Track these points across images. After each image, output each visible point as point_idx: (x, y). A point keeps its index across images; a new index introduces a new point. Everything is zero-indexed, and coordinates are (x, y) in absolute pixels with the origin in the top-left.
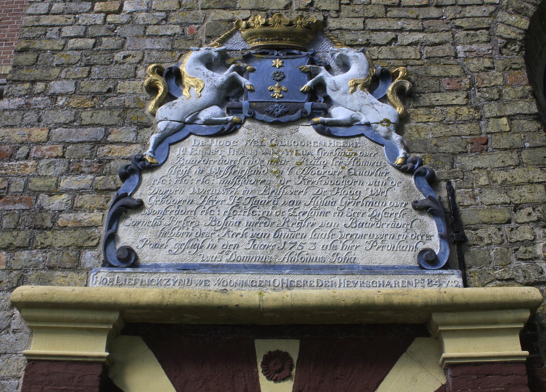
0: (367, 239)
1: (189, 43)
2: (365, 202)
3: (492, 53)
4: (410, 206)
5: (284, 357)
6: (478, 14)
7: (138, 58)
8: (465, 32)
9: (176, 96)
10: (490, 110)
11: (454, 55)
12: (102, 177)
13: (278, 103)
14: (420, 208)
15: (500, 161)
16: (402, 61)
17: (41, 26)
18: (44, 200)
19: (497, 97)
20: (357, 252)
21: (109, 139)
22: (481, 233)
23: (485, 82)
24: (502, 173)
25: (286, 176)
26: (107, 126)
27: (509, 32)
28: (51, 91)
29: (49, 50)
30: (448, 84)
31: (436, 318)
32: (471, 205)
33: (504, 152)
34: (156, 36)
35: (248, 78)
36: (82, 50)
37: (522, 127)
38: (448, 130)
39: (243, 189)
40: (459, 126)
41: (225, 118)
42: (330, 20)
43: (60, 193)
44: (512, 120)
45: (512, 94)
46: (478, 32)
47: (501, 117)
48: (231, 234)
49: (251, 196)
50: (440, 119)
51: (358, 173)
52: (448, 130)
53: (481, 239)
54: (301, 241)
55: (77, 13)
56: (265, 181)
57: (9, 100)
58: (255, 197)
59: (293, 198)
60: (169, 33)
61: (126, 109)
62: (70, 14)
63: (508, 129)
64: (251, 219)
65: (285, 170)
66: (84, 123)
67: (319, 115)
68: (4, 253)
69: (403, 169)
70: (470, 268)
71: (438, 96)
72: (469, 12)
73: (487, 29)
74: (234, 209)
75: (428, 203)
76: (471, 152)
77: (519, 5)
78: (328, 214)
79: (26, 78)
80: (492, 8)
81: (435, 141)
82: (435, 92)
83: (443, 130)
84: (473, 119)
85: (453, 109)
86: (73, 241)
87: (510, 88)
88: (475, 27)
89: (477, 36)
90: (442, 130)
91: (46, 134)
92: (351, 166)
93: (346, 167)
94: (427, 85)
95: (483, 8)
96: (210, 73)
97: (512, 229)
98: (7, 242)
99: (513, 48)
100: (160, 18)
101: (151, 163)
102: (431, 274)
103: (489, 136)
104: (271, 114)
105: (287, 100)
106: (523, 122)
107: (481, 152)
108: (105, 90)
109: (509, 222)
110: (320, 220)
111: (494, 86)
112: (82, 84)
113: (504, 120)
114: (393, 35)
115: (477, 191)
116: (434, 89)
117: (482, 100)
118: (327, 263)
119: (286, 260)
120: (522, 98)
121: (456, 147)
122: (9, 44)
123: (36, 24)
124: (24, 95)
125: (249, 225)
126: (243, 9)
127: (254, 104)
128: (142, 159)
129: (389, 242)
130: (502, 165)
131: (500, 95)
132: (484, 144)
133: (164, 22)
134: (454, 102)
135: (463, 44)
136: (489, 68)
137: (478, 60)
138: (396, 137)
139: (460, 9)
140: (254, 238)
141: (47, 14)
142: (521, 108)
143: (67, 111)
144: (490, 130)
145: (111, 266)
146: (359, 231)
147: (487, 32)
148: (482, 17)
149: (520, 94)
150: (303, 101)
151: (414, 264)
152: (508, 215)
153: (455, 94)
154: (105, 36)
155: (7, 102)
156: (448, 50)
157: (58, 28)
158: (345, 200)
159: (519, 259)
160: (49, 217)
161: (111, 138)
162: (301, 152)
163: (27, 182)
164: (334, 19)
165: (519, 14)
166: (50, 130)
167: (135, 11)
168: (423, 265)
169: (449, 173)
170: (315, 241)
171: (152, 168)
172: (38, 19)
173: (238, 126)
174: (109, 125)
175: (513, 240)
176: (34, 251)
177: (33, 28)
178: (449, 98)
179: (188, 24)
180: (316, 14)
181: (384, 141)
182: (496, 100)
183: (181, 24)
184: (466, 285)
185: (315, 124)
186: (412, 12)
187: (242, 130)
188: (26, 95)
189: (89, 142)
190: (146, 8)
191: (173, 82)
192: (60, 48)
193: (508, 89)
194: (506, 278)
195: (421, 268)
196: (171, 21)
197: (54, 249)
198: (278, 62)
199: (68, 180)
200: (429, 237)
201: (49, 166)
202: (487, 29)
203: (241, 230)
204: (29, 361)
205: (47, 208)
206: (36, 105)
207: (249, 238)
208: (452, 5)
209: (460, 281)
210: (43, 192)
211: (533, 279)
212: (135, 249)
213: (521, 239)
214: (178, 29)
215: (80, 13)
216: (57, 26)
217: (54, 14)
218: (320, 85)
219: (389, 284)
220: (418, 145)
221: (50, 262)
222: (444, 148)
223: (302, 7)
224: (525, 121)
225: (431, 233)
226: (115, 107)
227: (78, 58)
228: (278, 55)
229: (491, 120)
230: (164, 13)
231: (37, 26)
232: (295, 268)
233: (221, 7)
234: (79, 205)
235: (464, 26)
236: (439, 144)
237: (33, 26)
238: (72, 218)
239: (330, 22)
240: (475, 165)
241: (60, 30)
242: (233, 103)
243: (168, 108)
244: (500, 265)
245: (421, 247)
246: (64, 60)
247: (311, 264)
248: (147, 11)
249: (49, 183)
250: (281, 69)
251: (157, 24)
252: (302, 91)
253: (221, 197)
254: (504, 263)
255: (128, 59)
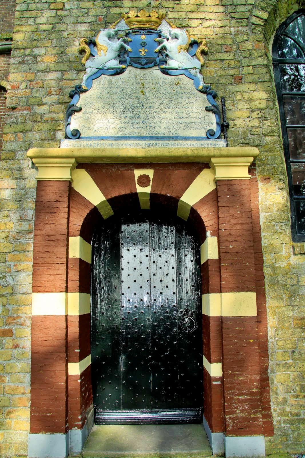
0: (184, 124)
1: (99, 26)
2: (183, 107)
3: (248, 32)
4: (204, 109)
5: (147, 177)
6: (243, 10)
7: (75, 35)
8: (236, 20)
9: (95, 55)
10: (245, 62)
11: (229, 33)
12: (62, 96)
13: (144, 58)
14: (207, 110)
15: (247, 88)
16: (204, 36)
17: (24, 18)
18: (37, 109)
19: (248, 56)
20: (180, 130)
21: (64, 78)
22: (236, 122)
23: (243, 48)
24: (247, 94)
25: (147, 94)
26: (62, 71)
27: (258, 21)
28: (34, 54)
29: (30, 31)
30: (226, 48)
31: (213, 160)
32: (233, 109)
33: (249, 84)
34: (82, 23)
35: (128, 45)
36: (47, 31)
37: (259, 72)
38: (224, 72)
39: (127, 101)
40: (229, 70)
41: (118, 66)
42: (169, 13)
43: (43, 105)
44: (254, 67)
45: (256, 54)
46: (242, 20)
47: (249, 66)
48: (122, 122)
49: (131, 104)
50: (221, 66)
51: (181, 93)
52: (224, 72)
53: (236, 125)
54: (154, 125)
55: (42, 10)
56: (138, 97)
57: (14, 59)
58: (133, 105)
59: (150, 105)
60: (89, 21)
61: (71, 62)
62: (38, 10)
63: (252, 72)
64: (132, 115)
65: (147, 92)
66: (51, 70)
67: (163, 64)
68: (21, 134)
69: (202, 91)
70: (230, 138)
71: (220, 55)
72: (239, 9)
73: (247, 19)
74: (124, 110)
75: (212, 108)
76: (234, 83)
77: (264, 5)
78: (167, 113)
79: (21, 47)
80: (250, 7)
81: (217, 78)
82: (219, 53)
83: (222, 72)
84: (236, 67)
85: (227, 62)
86: (51, 127)
87: (255, 51)
88: (241, 18)
89: (241, 22)
90: (220, 72)
91: (34, 76)
92: (177, 90)
93: (175, 90)
94: (215, 49)
95: (246, 7)
96: (110, 42)
97: (250, 121)
98: (22, 129)
99: (259, 29)
100: (84, 12)
101: (85, 89)
102: (211, 141)
103: (243, 75)
104: (140, 64)
105: (148, 57)
106: (259, 69)
107: (239, 83)
108: (60, 53)
109: (249, 117)
110: (163, 115)
111: (247, 50)
112: (49, 50)
113: (251, 68)
114: (201, 22)
115: (235, 102)
116: (218, 51)
117: (241, 57)
118: (166, 135)
119: (147, 134)
120: (260, 56)
121: (227, 80)
122: (4, 21)
123: (22, 16)
124: (21, 56)
125: (131, 118)
126: (126, 7)
127: (132, 59)
128: (80, 87)
129: (194, 126)
130: (248, 90)
131: (250, 55)
132: (240, 80)
133: (86, 15)
134: (228, 58)
135: (234, 27)
136: (247, 40)
137: (241, 36)
138: (200, 76)
139: (234, 7)
140: (133, 124)
141: (26, 11)
142: (260, 62)
143: (42, 64)
144: (243, 72)
145: (70, 138)
146: (181, 121)
147: (247, 21)
148: (245, 12)
149: (260, 54)
150: (155, 57)
151: (205, 136)
152: (248, 115)
153: (228, 54)
154: (57, 23)
155: (13, 60)
156: (227, 30)
157: (33, 19)
158: (174, 106)
159: (251, 135)
160: (39, 116)
161: (64, 77)
162: (154, 83)
163: (28, 100)
164: (171, 13)
165: (264, 10)
166: (35, 73)
167: (71, 9)
168: (209, 137)
169: (223, 94)
170: (161, 125)
171: (84, 91)
172: (22, 14)
173: (124, 70)
174: (63, 71)
175: (250, 126)
176: (35, 132)
177: (21, 19)
178: (226, 56)
179: (98, 16)
180: (162, 10)
181: (194, 78)
182: (248, 57)
183: (95, 16)
184: (227, 146)
185: (161, 69)
186: (210, 9)
187: (126, 72)
188: (22, 56)
189: (55, 79)
190: (76, 6)
191: (92, 46)
192: (36, 30)
193: (254, 52)
194: (245, 143)
195: (208, 138)
196: (90, 14)
197: (43, 131)
198: (143, 37)
199: (46, 98)
200: (212, 124)
201: (37, 92)
202: (247, 19)
203: (127, 120)
204: (38, 181)
205: (38, 112)
206: (27, 61)
207: (130, 124)
208: (231, 5)
209: (225, 144)
210: (35, 104)
211: (257, 144)
212: (79, 130)
213: (253, 126)
214: (93, 19)
215: (44, 10)
216: (33, 17)
217: (30, 11)
218: (164, 48)
219: (193, 145)
220: (209, 79)
221: (42, 137)
222: (222, 81)
223: (155, 6)
224: (260, 69)
225: (213, 122)
226: (66, 61)
227: (45, 36)
228: (143, 33)
229: (245, 68)
230: (86, 10)
231: (22, 18)
232: (152, 138)
233: (114, 6)
234: (52, 110)
235: (235, 17)
236: (219, 79)
237: (20, 18)
238: (50, 117)
239: (169, 14)
240: (236, 90)
241: (34, 20)
242: (122, 58)
243: (91, 61)
244: (243, 137)
245: (208, 128)
246: (38, 37)
247: (158, 136)
248: (77, 9)
249: (38, 100)
250: (145, 41)
251: (83, 16)
252: (155, 52)
253: (117, 105)
254: (245, 136)
255: (69, 36)
